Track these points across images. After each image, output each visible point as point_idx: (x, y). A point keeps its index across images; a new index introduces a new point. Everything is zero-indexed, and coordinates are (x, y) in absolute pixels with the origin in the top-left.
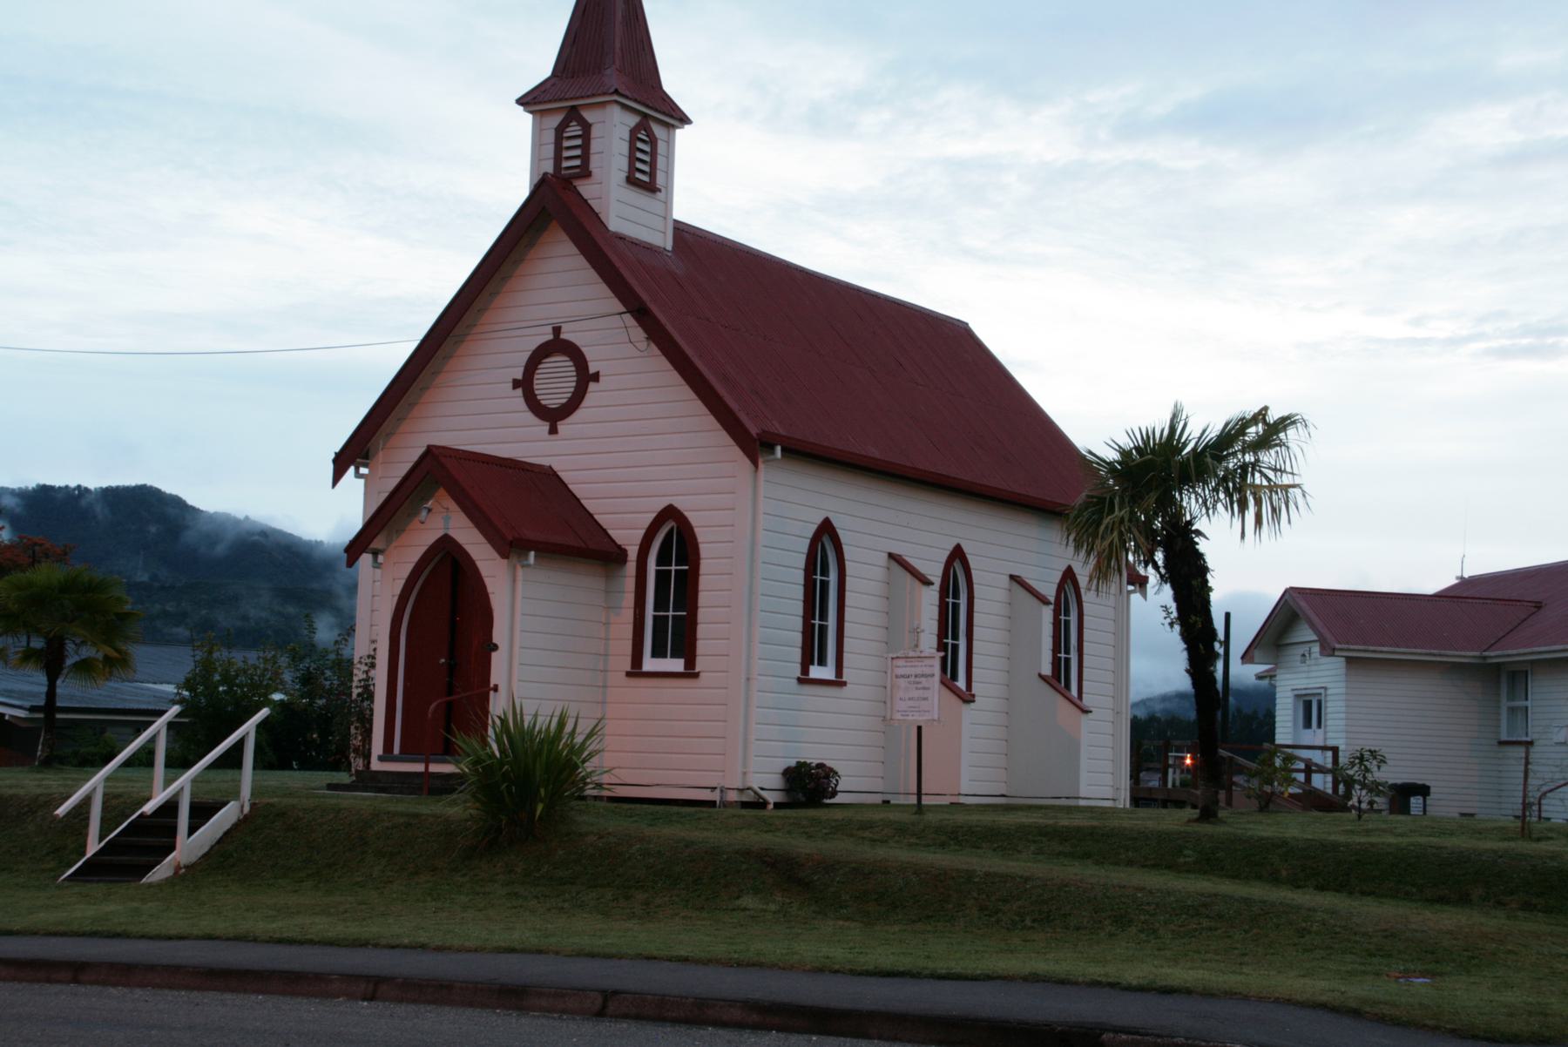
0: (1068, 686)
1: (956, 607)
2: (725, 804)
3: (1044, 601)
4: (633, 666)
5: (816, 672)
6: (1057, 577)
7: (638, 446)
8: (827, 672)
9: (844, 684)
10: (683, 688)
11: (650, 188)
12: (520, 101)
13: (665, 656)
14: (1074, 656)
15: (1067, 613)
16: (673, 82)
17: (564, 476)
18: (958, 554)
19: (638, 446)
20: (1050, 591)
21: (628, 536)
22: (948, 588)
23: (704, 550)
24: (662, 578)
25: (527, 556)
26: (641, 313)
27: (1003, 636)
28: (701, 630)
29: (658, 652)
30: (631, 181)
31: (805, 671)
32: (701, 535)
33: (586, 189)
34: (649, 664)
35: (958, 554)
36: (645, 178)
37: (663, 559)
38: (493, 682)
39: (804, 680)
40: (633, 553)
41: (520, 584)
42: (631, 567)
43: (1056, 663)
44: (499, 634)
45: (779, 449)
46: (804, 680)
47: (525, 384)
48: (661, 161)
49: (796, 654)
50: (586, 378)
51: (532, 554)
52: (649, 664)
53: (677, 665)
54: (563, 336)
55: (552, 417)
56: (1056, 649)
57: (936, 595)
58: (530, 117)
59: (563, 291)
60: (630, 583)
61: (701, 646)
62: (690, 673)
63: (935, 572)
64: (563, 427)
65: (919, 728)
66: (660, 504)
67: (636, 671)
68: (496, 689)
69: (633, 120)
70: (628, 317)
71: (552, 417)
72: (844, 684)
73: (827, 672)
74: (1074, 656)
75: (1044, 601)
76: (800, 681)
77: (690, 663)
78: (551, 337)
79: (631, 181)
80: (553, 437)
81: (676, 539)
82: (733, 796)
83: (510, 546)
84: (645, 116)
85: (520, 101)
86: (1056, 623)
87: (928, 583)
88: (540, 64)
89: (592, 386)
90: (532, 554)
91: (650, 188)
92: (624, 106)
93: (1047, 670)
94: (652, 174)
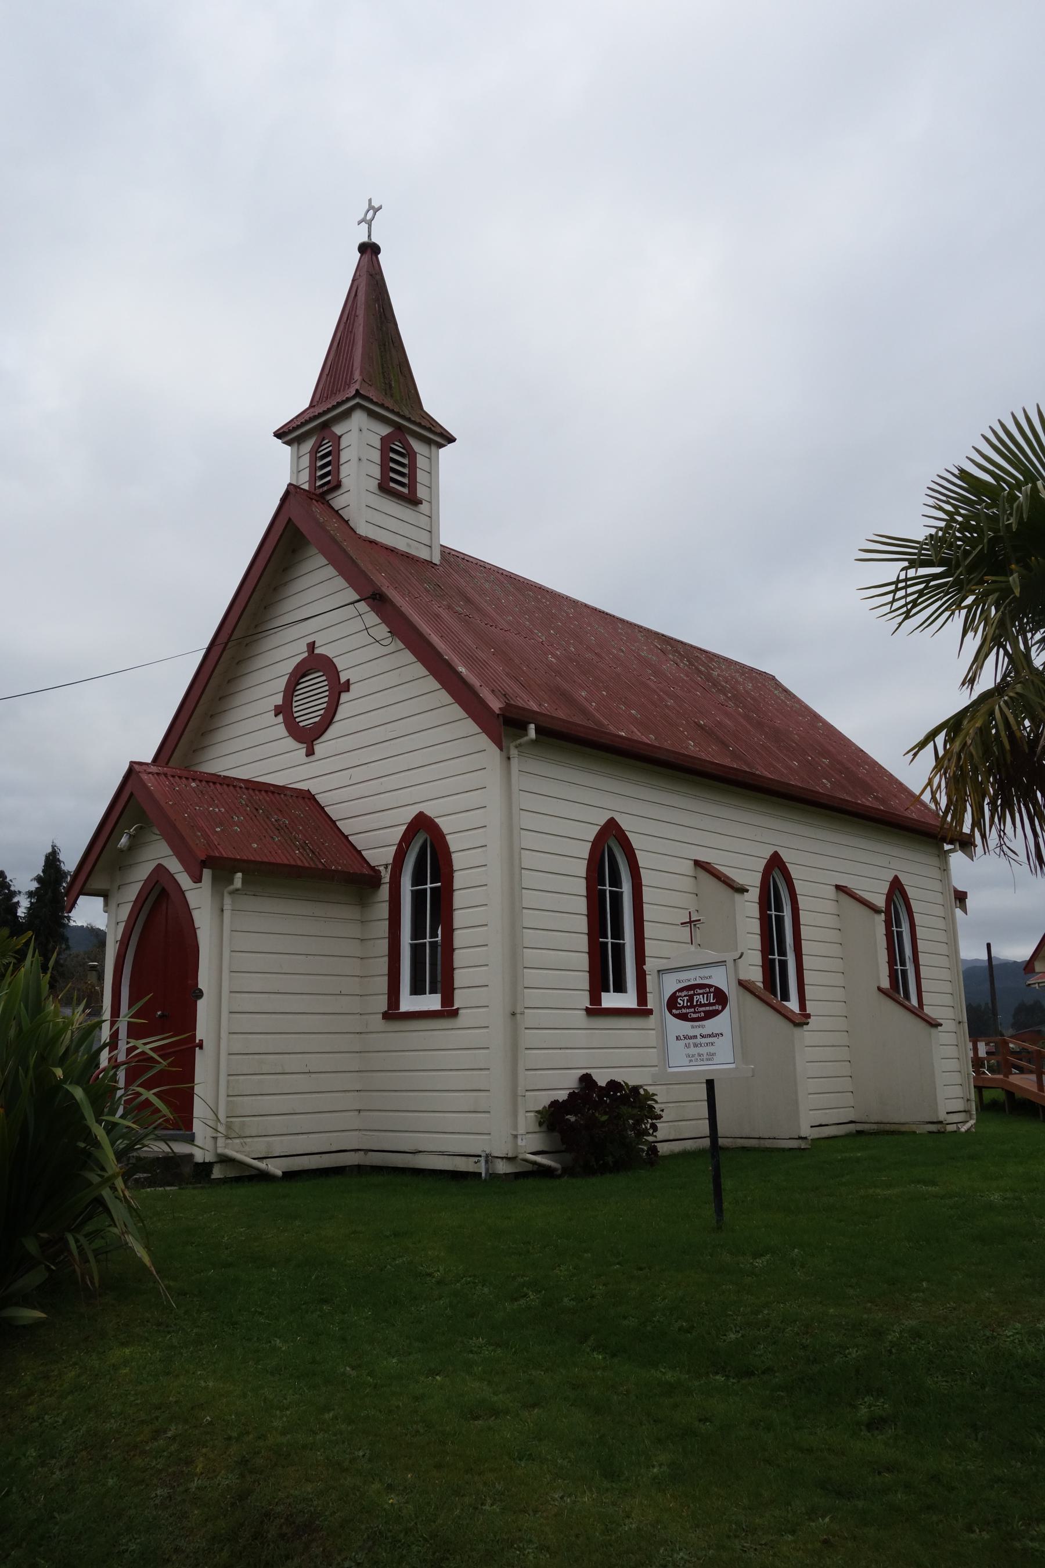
0: (907, 996)
1: (780, 920)
2: (494, 1177)
3: (876, 911)
4: (389, 1008)
5: (610, 1000)
6: (885, 888)
7: (394, 757)
8: (627, 1000)
9: (650, 1012)
10: (438, 1033)
11: (412, 500)
12: (279, 435)
13: (423, 992)
14: (910, 967)
15: (899, 925)
16: (436, 399)
17: (322, 799)
18: (776, 864)
19: (394, 757)
20: (880, 902)
21: (381, 856)
22: (769, 899)
23: (458, 861)
24: (418, 898)
25: (231, 882)
26: (377, 600)
27: (834, 952)
28: (460, 958)
29: (417, 989)
30: (384, 488)
31: (595, 999)
32: (454, 843)
33: (339, 501)
34: (408, 1003)
35: (776, 864)
36: (405, 491)
37: (418, 878)
38: (199, 1036)
39: (595, 1011)
40: (386, 877)
41: (227, 914)
42: (384, 891)
43: (893, 975)
44: (205, 980)
45: (532, 726)
46: (595, 1011)
47: (285, 710)
48: (421, 476)
49: (583, 980)
50: (338, 688)
51: (239, 875)
52: (408, 1003)
53: (432, 1002)
54: (317, 651)
55: (308, 737)
56: (892, 962)
57: (754, 910)
58: (288, 448)
59: (323, 612)
60: (383, 910)
61: (460, 978)
62: (449, 1012)
63: (752, 880)
64: (321, 748)
65: (710, 1084)
66: (408, 815)
67: (393, 1014)
68: (201, 1046)
69: (385, 430)
70: (363, 606)
71: (308, 737)
72: (650, 1012)
73: (627, 1000)
74: (910, 967)
75: (876, 911)
76: (589, 1012)
77: (448, 999)
78: (306, 654)
79: (384, 488)
80: (312, 758)
81: (427, 847)
82: (502, 1168)
83: (218, 867)
84: (399, 427)
85: (279, 435)
86: (889, 934)
87: (742, 890)
88: (296, 397)
89: (344, 697)
90: (239, 875)
91: (412, 500)
92: (371, 414)
93: (886, 984)
94: (413, 485)
